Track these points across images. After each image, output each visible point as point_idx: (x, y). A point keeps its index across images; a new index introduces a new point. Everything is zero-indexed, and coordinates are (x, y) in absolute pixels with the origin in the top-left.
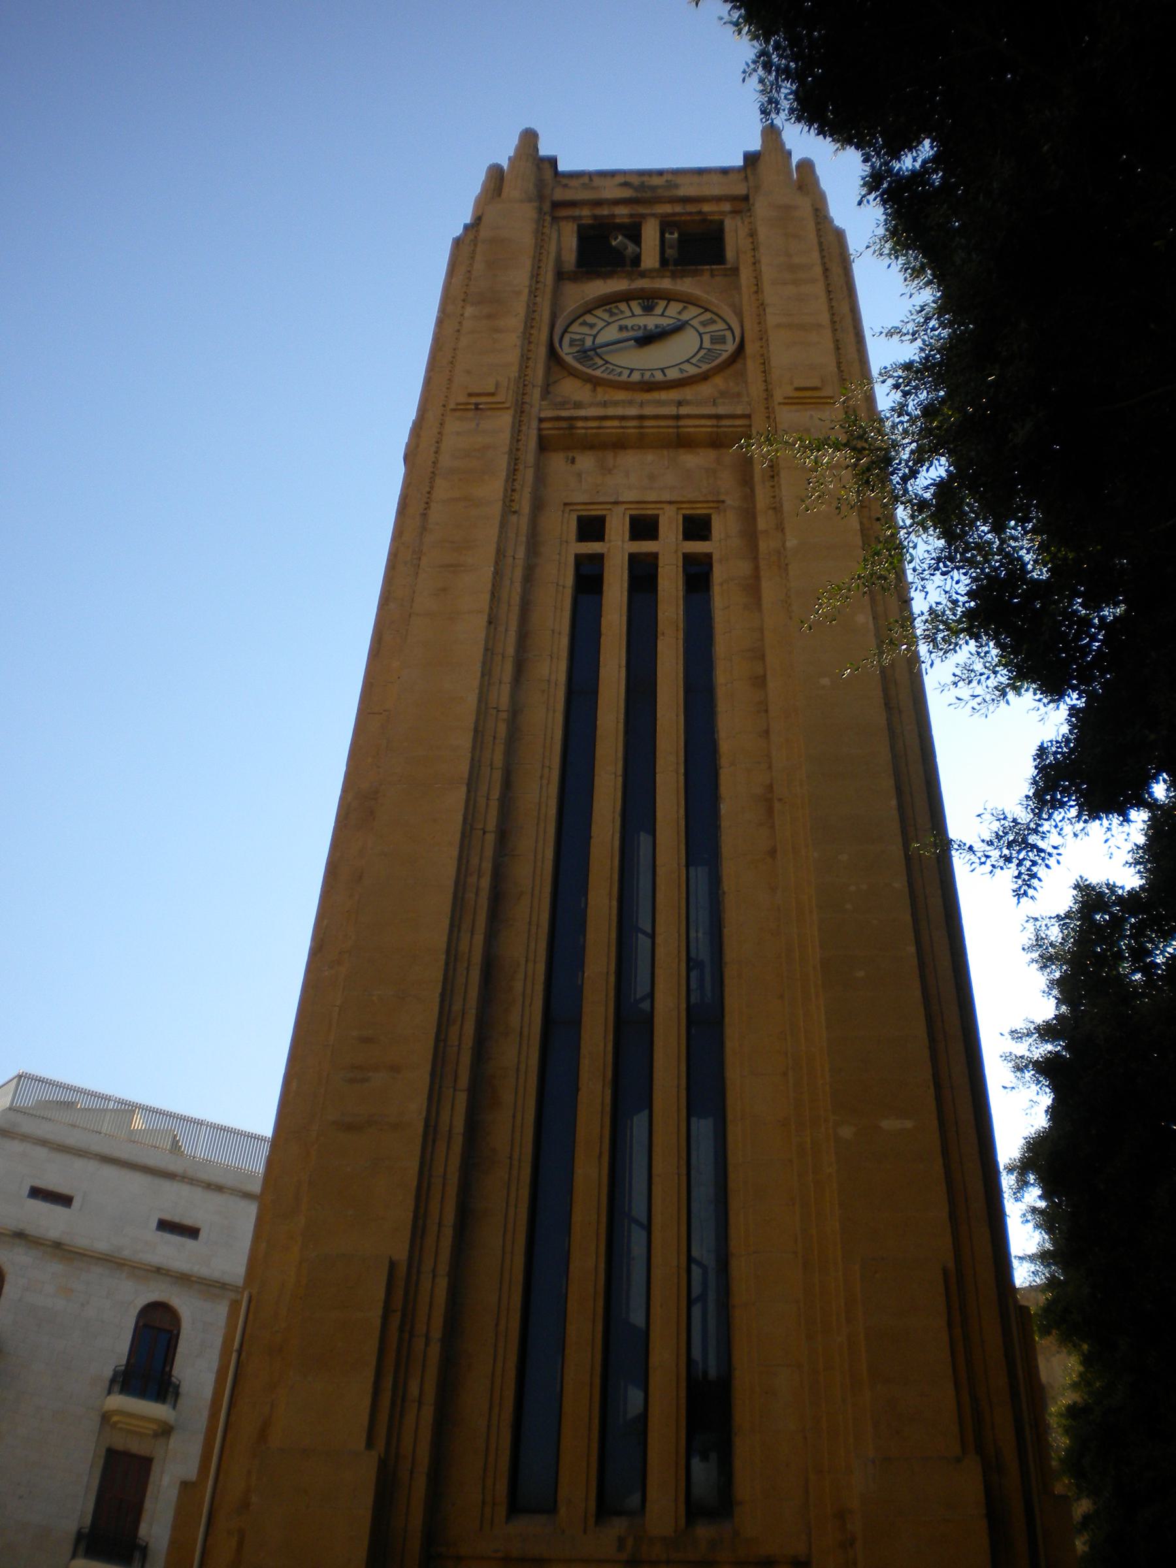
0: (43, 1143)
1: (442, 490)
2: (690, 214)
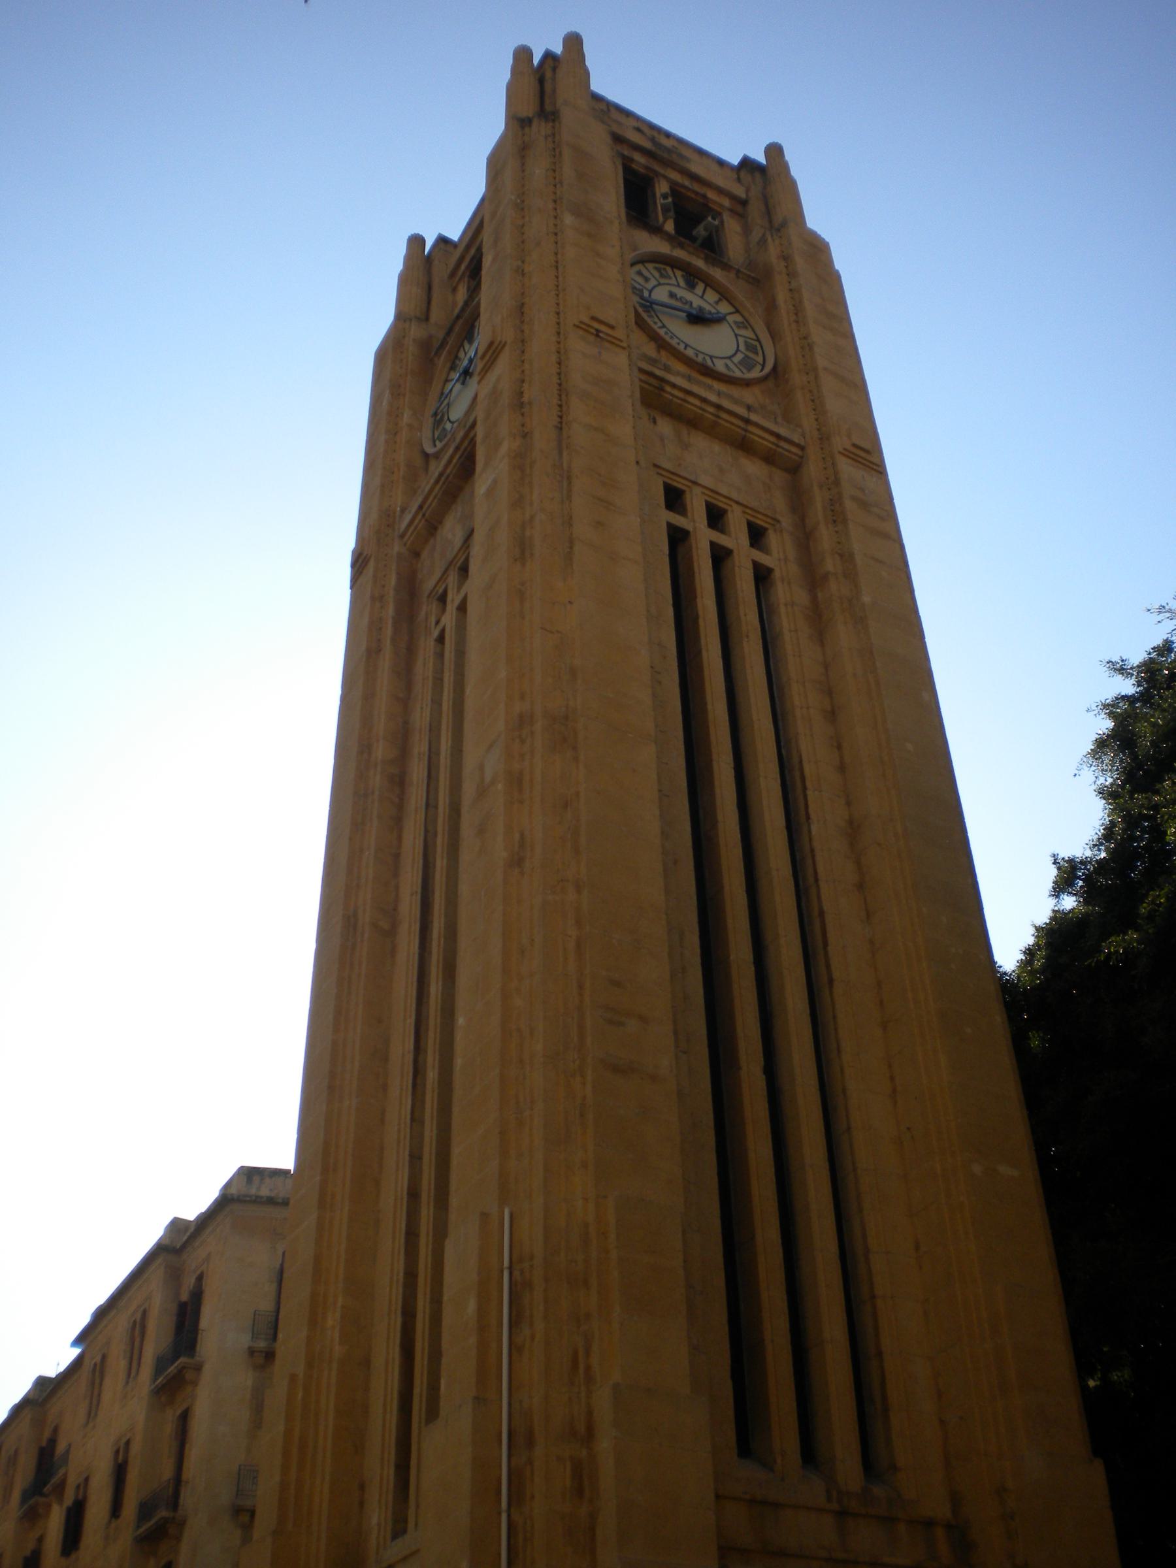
2: (697, 193)
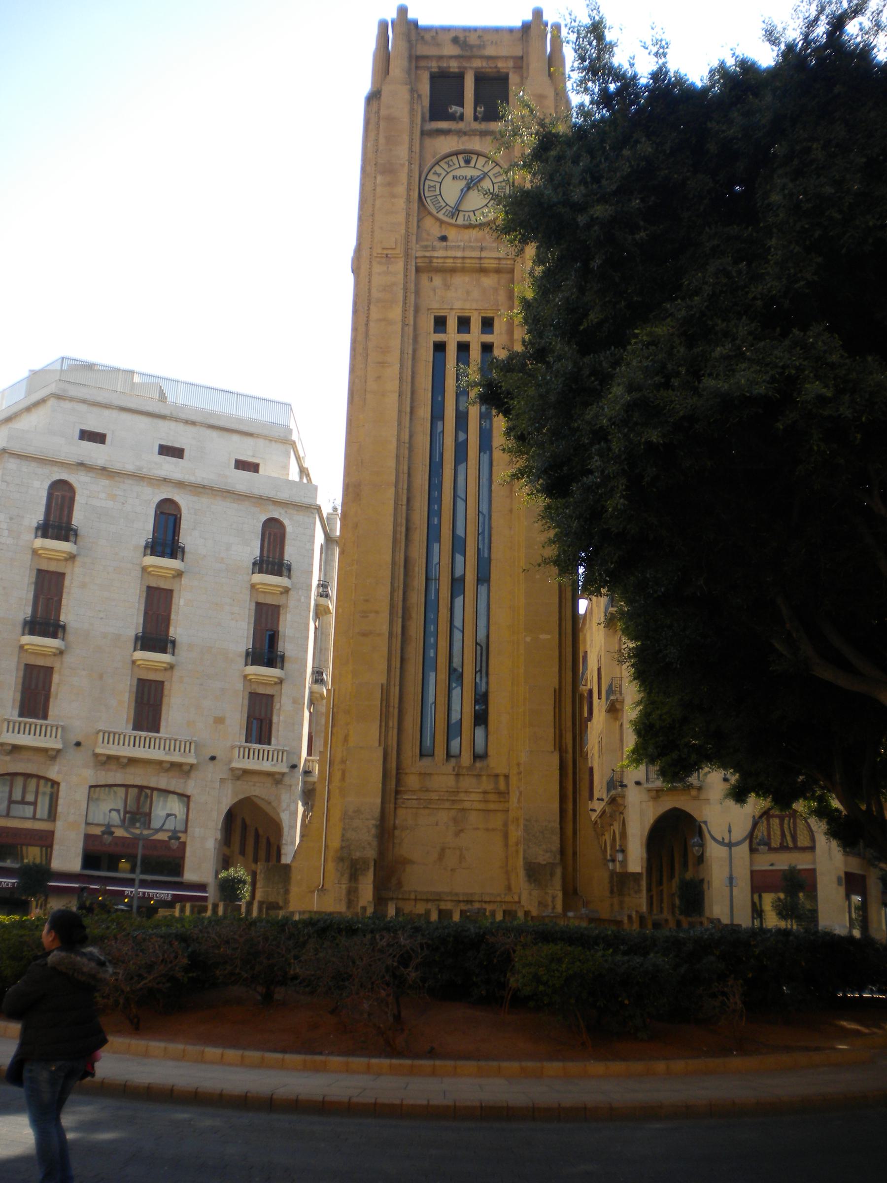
0: (84, 401)
1: (375, 314)
